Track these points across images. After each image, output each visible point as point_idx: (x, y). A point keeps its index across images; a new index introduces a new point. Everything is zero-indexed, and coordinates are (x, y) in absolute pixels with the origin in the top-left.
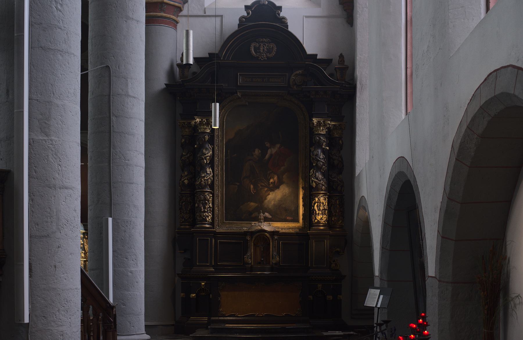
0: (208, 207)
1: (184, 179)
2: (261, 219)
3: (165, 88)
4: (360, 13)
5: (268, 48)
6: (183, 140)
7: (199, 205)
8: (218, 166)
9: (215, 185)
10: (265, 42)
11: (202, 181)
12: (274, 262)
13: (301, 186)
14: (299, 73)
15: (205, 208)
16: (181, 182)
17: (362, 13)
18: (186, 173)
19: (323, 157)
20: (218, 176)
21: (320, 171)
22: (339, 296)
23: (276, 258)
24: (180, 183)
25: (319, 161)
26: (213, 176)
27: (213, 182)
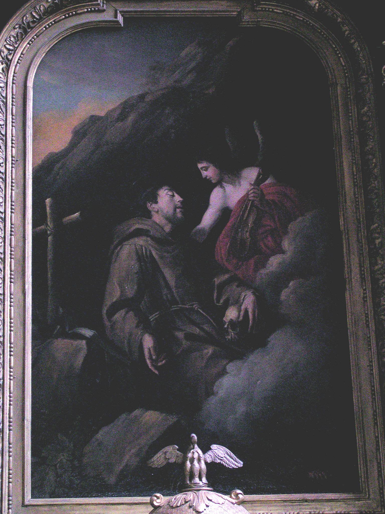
2: (197, 474)
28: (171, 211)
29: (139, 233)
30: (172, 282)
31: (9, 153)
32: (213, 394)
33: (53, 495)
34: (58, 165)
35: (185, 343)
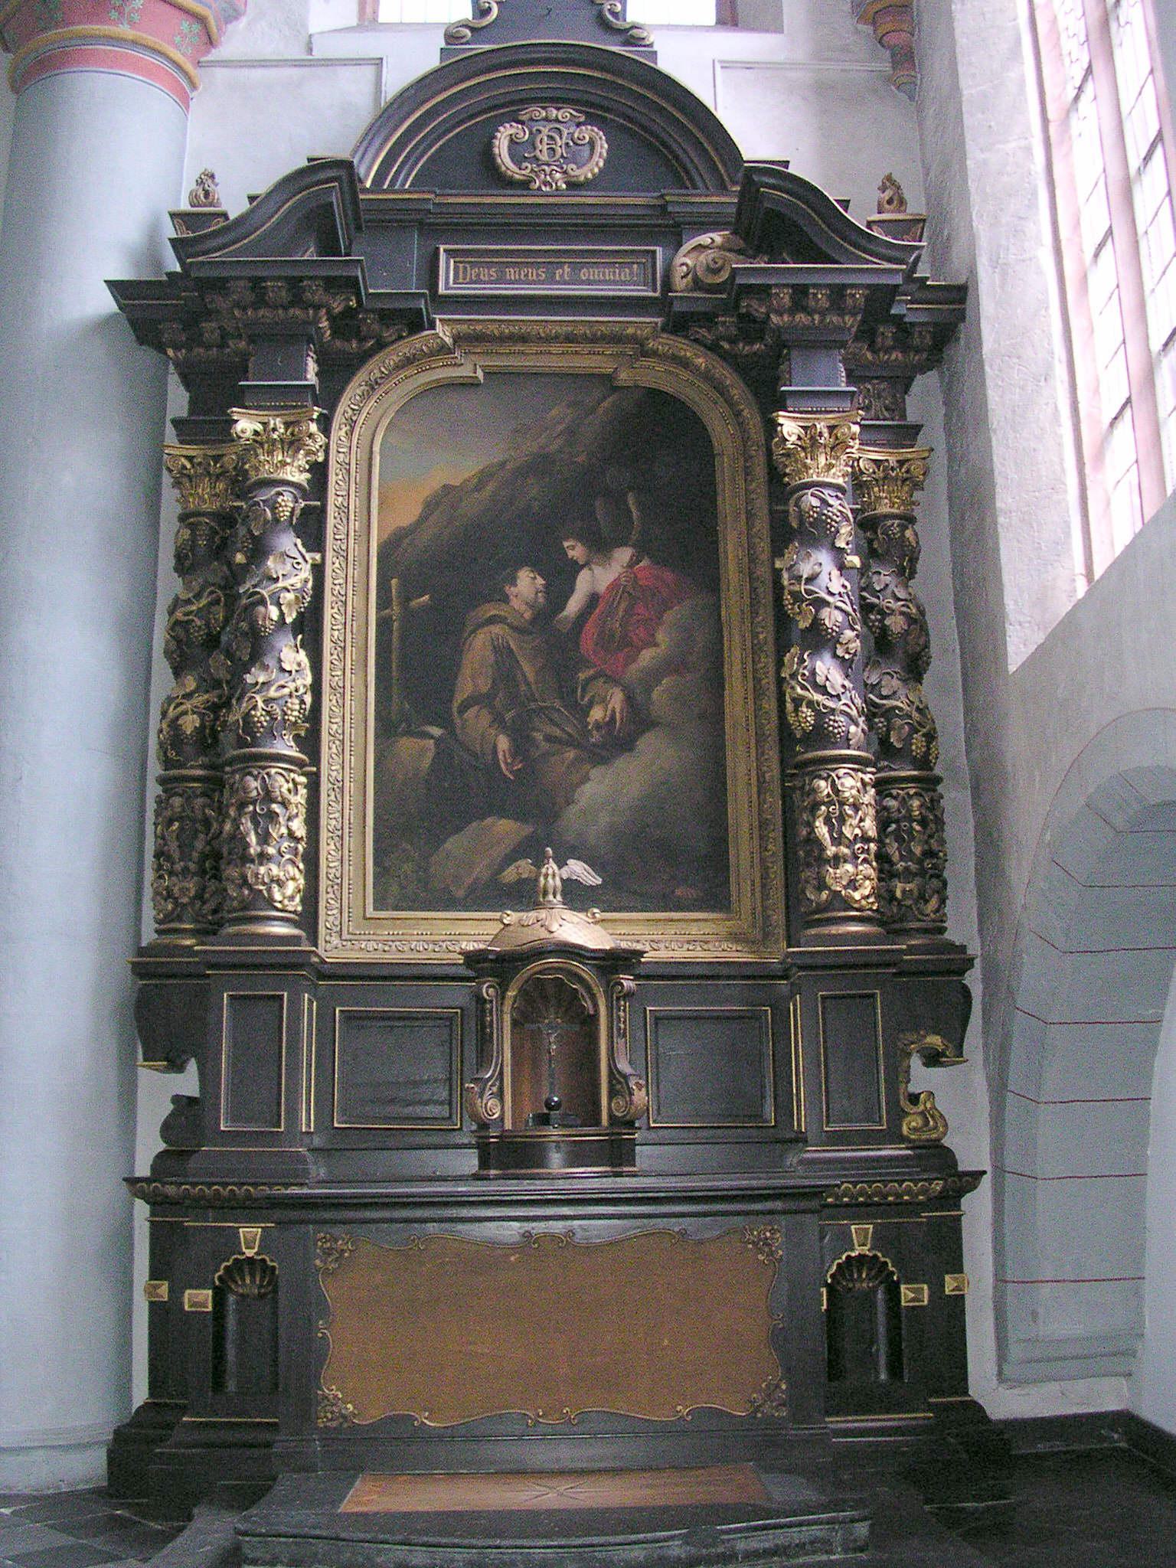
1: (180, 709)
2: (551, 891)
3: (117, 314)
8: (344, 648)
9: (325, 737)
10: (557, 120)
11: (255, 707)
15: (265, 838)
16: (164, 726)
19: (844, 586)
21: (835, 656)
25: (828, 604)
26: (316, 688)
29: (492, 620)
30: (531, 676)
31: (351, 526)
33: (396, 908)
34: (407, 541)
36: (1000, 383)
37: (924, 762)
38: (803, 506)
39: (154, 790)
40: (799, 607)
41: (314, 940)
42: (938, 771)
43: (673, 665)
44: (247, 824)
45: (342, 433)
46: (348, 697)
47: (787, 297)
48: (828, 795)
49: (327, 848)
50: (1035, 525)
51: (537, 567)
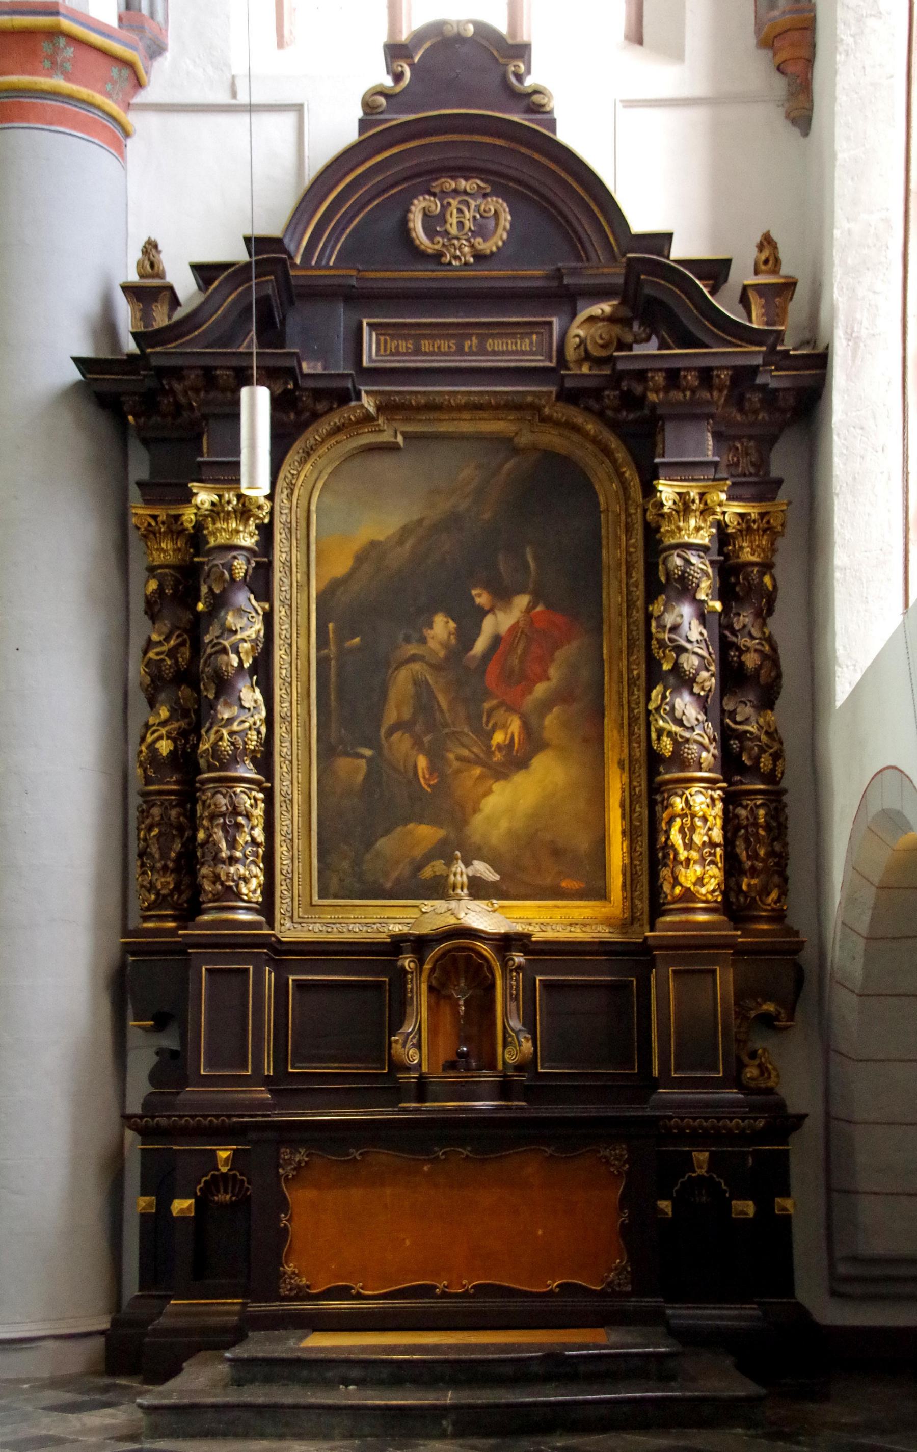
0: (246, 843)
1: (156, 735)
3: (80, 382)
4: (848, 45)
5: (478, 216)
6: (153, 585)
7: (210, 836)
8: (291, 684)
9: (277, 759)
10: (465, 192)
11: (221, 739)
12: (511, 1058)
13: (616, 760)
14: (600, 312)
15: (232, 844)
16: (143, 748)
17: (855, 42)
18: (164, 713)
19: (701, 634)
20: (291, 723)
21: (692, 693)
22: (778, 1200)
23: (520, 1045)
24: (141, 752)
25: (685, 650)
26: (269, 721)
27: (268, 742)
28: (446, 637)
29: (413, 658)
32: (480, 810)
35: (456, 764)
36: (845, 451)
37: (771, 778)
38: (669, 565)
39: (135, 800)
40: (664, 652)
41: (271, 924)
42: (784, 784)
43: (562, 696)
44: (219, 834)
45: (284, 496)
46: (295, 723)
47: (661, 379)
48: (682, 809)
49: (281, 849)
50: (864, 581)
51: (451, 614)
